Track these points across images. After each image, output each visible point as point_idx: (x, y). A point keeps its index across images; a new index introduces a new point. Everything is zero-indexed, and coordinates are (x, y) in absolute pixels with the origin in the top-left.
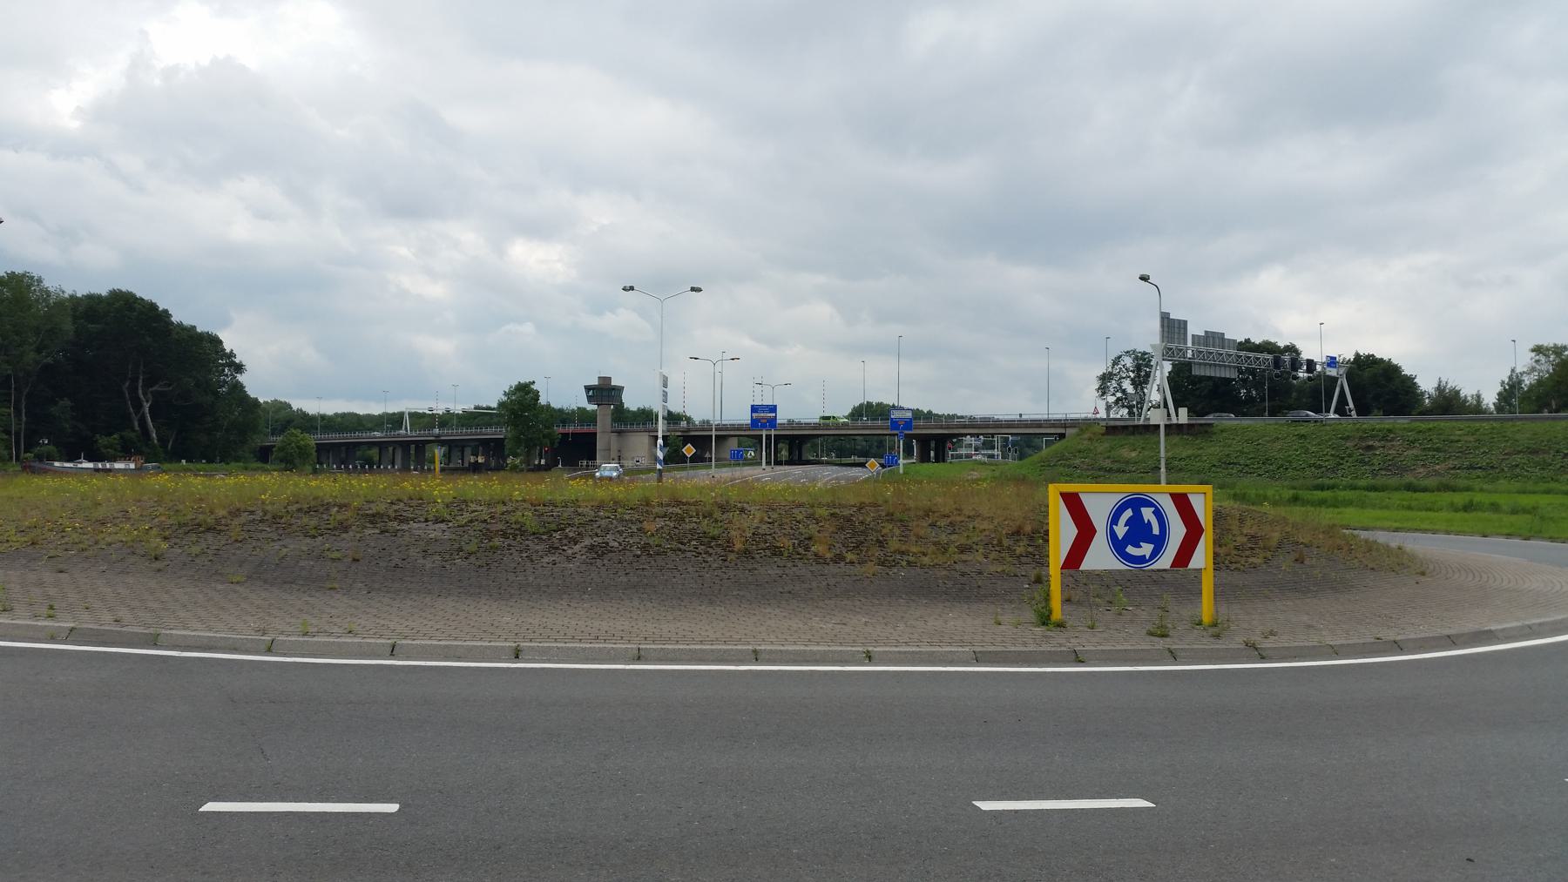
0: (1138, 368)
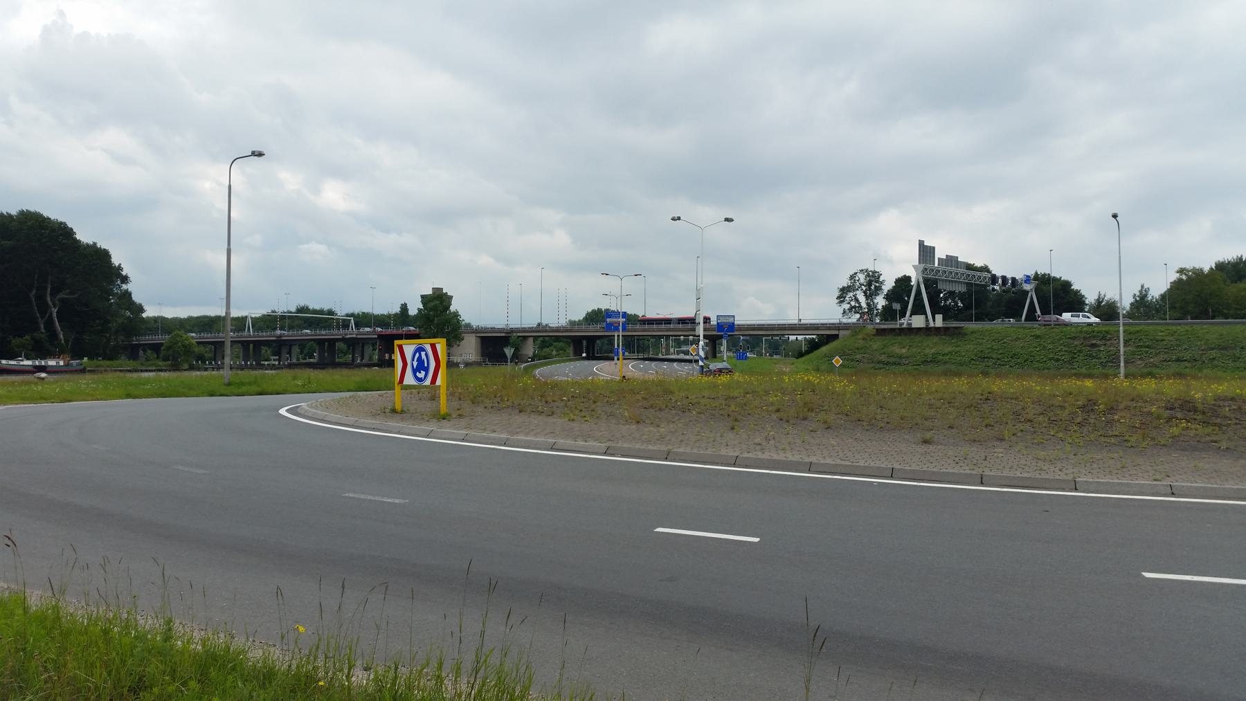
0: (869, 284)
